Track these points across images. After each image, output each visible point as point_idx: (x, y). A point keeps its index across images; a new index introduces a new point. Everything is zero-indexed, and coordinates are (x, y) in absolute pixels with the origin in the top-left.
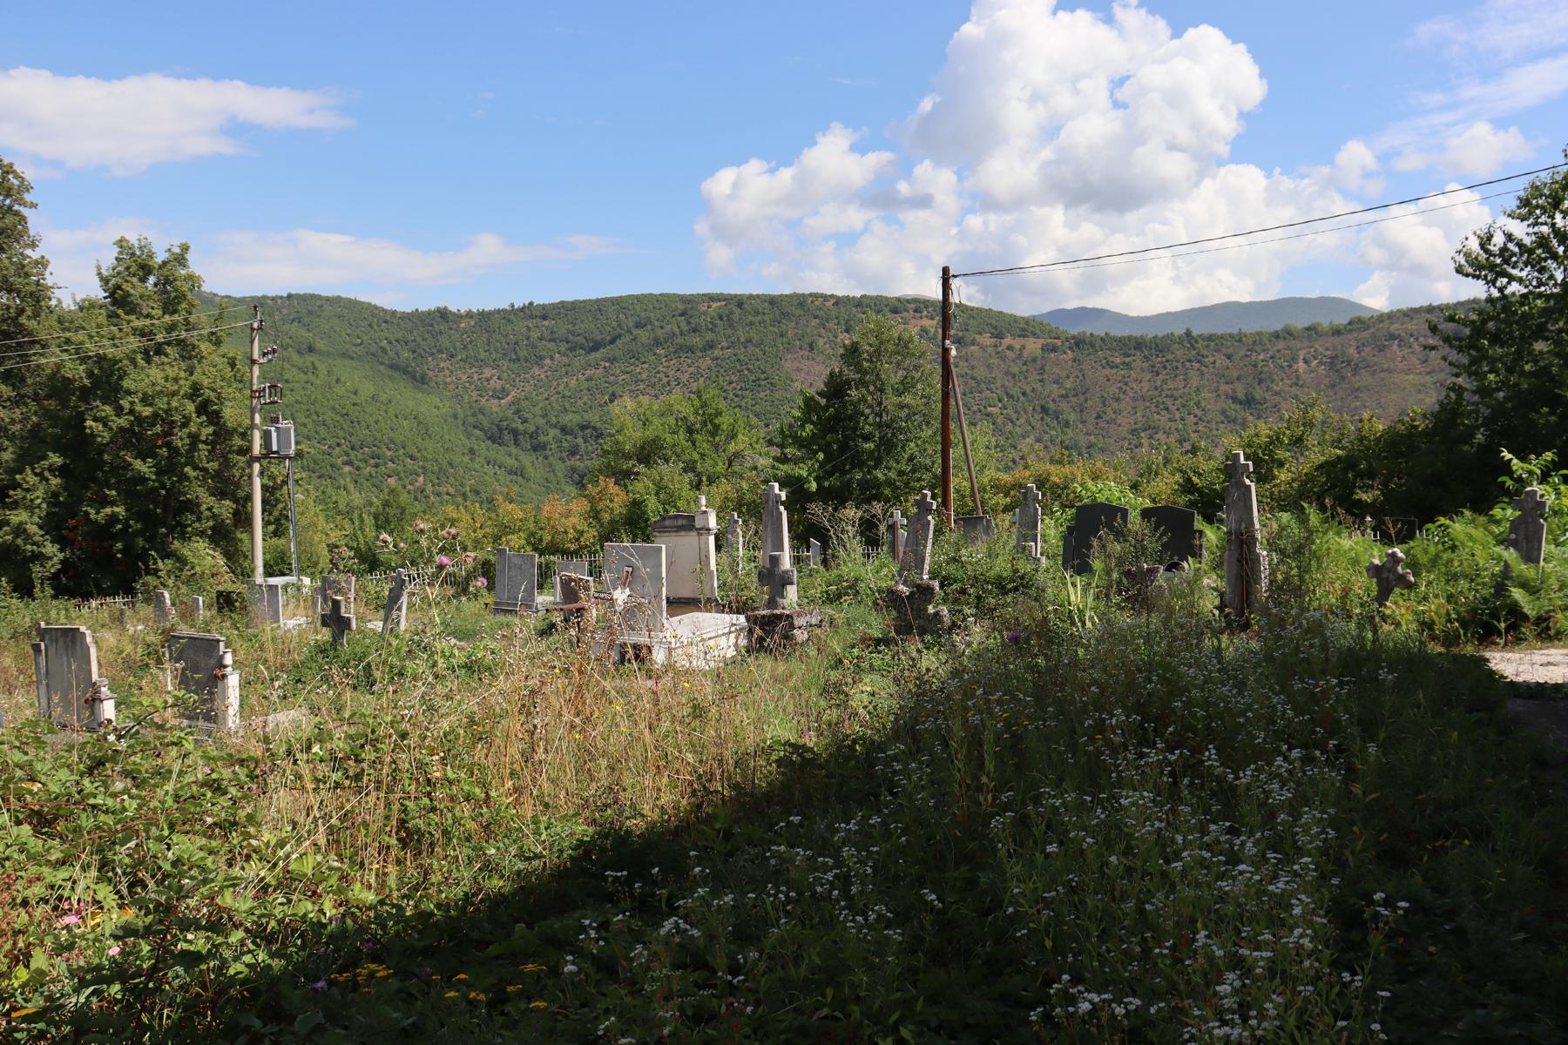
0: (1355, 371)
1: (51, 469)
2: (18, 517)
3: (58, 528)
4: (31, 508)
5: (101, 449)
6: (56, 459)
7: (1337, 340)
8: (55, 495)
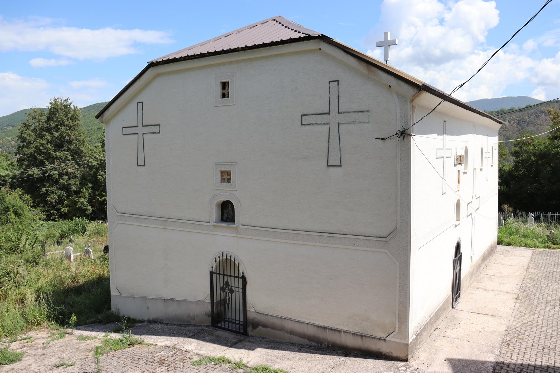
0: (528, 125)
1: (89, 188)
2: (82, 200)
3: (91, 202)
4: (84, 197)
5: (101, 183)
6: (90, 185)
7: (520, 114)
8: (90, 194)
